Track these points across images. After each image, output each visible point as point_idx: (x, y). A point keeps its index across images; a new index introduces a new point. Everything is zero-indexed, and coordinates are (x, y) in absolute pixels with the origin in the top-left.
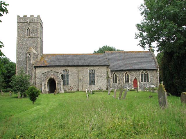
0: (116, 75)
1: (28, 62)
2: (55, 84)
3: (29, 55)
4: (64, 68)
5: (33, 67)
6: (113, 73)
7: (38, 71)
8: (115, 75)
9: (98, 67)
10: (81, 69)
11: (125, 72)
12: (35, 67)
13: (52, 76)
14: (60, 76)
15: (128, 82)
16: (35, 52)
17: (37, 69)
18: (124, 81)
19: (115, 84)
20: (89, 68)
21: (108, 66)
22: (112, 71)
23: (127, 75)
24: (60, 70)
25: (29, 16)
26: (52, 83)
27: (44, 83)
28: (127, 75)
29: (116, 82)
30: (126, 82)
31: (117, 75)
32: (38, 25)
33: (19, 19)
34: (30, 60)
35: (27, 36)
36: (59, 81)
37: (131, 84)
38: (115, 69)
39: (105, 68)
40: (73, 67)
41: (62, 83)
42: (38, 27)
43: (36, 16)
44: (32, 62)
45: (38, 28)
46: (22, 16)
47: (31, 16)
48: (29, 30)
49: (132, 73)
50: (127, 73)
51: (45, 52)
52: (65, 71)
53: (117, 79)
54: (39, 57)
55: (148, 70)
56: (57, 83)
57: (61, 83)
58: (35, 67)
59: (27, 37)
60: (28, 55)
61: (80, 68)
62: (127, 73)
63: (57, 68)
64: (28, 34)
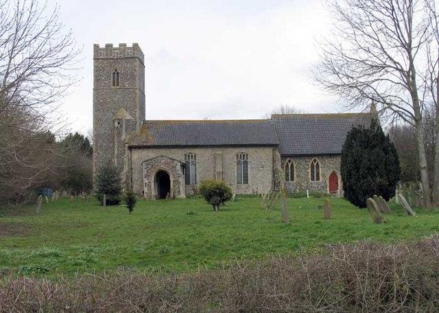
0: (292, 166)
1: (116, 137)
2: (170, 181)
3: (119, 123)
4: (187, 151)
5: (126, 148)
6: (287, 161)
7: (137, 156)
8: (290, 165)
9: (253, 150)
10: (221, 153)
11: (313, 159)
12: (131, 148)
13: (164, 167)
14: (179, 167)
15: (318, 179)
16: (129, 117)
17: (133, 151)
18: (310, 177)
19: (290, 184)
20: (237, 151)
21: (274, 146)
22: (284, 157)
23: (315, 164)
24: (179, 155)
25: (116, 45)
26: (163, 180)
27: (148, 180)
28: (315, 164)
29: (292, 179)
30: (313, 179)
31: (295, 166)
32: (135, 64)
33: (97, 52)
34: (119, 134)
35: (114, 85)
36: (177, 178)
37: (323, 184)
38: (292, 152)
39: (269, 151)
40: (205, 149)
41: (182, 180)
42: (135, 66)
43: (130, 45)
44: (123, 137)
45: (135, 70)
46: (102, 46)
47: (120, 45)
48: (118, 73)
49: (327, 160)
50: (315, 161)
51: (148, 118)
52: (189, 156)
53: (295, 173)
54: (138, 127)
55: (318, 155)
56: (172, 179)
57: (180, 180)
58: (131, 148)
59: (113, 87)
60: (116, 125)
61: (219, 151)
62: (315, 161)
63: (173, 150)
64: (116, 83)
